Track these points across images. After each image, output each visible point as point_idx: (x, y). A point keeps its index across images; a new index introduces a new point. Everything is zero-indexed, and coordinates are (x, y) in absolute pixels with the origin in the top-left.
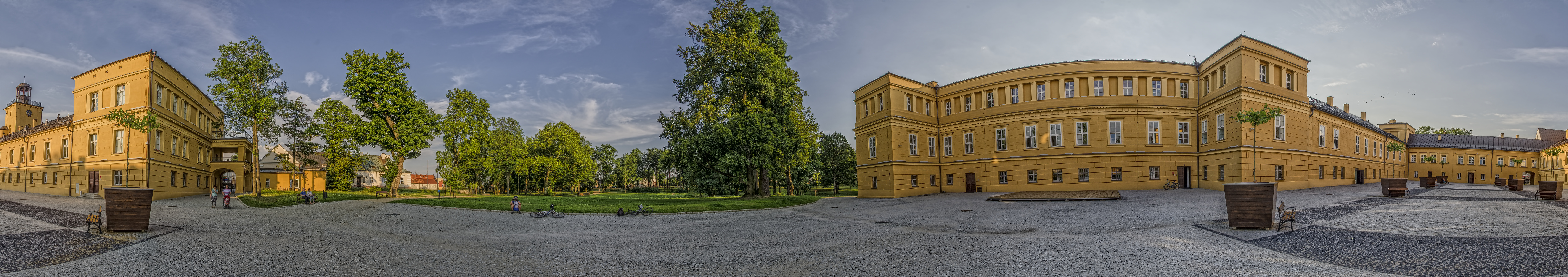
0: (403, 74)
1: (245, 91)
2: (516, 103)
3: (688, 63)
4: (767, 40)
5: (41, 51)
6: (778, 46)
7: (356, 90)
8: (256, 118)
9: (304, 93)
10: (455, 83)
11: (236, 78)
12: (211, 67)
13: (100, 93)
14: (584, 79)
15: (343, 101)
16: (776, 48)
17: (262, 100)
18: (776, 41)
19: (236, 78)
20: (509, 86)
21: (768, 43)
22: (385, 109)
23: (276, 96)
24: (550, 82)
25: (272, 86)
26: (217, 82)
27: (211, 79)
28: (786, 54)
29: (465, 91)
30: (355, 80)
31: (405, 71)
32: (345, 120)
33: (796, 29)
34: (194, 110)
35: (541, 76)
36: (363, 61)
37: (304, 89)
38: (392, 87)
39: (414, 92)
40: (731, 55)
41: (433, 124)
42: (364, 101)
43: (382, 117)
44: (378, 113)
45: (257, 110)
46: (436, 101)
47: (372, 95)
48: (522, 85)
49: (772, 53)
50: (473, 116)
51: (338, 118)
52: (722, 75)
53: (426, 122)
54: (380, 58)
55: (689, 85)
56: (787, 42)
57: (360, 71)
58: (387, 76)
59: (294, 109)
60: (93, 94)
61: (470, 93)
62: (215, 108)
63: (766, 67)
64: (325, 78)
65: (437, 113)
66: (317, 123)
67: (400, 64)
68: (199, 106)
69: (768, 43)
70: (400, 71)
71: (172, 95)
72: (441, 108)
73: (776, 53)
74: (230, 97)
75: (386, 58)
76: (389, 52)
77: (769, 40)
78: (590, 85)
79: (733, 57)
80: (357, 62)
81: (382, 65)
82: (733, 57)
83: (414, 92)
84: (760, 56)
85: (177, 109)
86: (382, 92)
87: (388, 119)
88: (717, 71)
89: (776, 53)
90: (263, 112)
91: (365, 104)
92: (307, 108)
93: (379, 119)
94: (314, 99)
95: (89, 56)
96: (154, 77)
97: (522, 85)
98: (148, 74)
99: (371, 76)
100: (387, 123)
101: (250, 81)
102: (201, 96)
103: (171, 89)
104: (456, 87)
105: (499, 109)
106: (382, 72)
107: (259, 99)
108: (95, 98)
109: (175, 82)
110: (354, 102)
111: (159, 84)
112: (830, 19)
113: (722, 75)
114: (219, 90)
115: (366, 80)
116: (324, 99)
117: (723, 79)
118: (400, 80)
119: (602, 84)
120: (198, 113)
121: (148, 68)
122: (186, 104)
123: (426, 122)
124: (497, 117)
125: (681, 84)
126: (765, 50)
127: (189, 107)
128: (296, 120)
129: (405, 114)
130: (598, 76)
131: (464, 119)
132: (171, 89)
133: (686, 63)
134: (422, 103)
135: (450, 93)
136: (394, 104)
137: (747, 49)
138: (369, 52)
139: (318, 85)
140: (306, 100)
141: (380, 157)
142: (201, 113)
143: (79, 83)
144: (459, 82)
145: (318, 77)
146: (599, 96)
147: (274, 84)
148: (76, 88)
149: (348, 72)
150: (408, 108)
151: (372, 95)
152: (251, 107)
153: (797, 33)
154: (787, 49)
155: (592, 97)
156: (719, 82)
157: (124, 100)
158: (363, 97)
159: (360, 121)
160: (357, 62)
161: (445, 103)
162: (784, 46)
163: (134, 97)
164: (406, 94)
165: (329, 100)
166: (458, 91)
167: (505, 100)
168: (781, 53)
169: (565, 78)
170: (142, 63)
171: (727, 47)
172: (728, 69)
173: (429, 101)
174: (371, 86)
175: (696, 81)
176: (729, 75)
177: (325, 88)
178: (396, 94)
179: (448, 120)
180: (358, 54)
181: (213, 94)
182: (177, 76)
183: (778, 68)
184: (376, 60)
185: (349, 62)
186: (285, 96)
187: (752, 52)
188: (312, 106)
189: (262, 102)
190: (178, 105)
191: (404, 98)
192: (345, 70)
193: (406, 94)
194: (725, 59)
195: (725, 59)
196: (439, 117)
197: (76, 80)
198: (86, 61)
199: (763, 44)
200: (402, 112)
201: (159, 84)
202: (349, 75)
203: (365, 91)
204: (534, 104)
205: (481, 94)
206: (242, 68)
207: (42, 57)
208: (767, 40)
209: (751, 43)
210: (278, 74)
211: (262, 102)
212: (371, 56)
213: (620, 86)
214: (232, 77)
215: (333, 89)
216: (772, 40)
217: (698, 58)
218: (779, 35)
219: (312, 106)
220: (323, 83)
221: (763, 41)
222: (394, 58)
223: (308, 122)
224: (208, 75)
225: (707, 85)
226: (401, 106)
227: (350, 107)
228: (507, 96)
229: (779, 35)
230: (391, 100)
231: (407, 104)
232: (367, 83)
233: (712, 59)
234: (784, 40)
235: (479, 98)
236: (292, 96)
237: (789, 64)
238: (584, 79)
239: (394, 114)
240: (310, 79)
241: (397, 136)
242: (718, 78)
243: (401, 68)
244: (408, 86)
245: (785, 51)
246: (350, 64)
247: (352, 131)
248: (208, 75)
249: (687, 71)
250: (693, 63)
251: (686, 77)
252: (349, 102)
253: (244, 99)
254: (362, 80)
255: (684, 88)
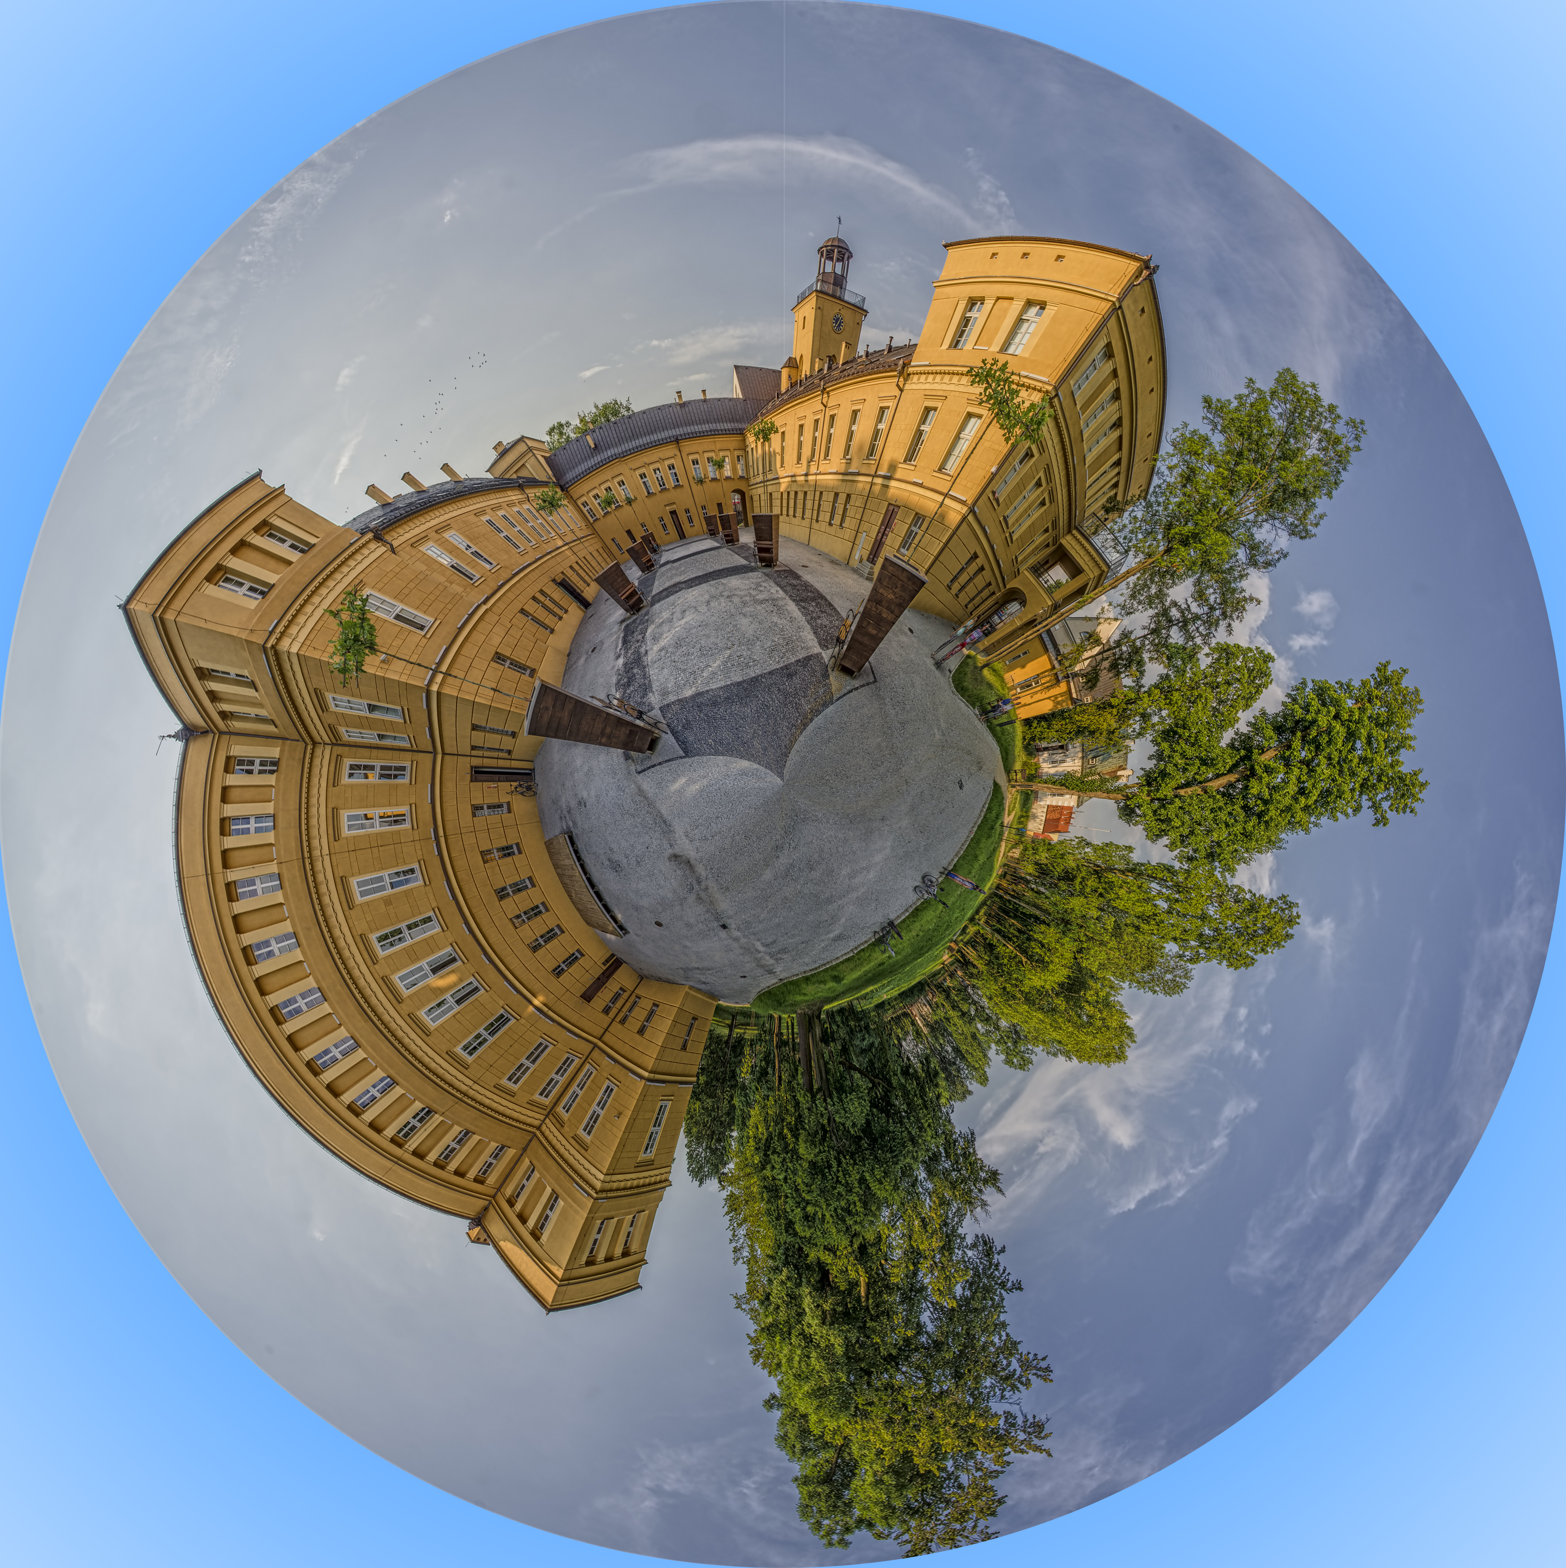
0: (1357, 809)
1: (1221, 494)
2: (1217, 1019)
3: (1010, 1347)
4: (830, 1454)
5: (887, 154)
6: (800, 1437)
7: (1306, 708)
8: (1168, 551)
9: (1272, 604)
10: (1317, 921)
11: (1240, 454)
12: (1229, 389)
13: (989, 304)
14: (1188, 1175)
15: (1273, 687)
16: (805, 1432)
17: (1219, 537)
18: (804, 1450)
19: (1240, 454)
20: (1266, 1029)
21: (826, 1445)
22: (1259, 770)
23: (1242, 555)
24: (1231, 1110)
25: (1263, 534)
26: (1205, 429)
27: (1201, 412)
28: (777, 1414)
29: (1288, 936)
30: (1336, 703)
31: (1367, 814)
32: (1221, 702)
33: (749, 1486)
34: (1115, 447)
35: (1253, 1104)
36: (1391, 713)
37: (1284, 601)
38: (1321, 785)
39: (1307, 831)
40: (916, 1399)
41: (1211, 856)
42: (1279, 729)
43: (1235, 766)
44: (1248, 757)
45: (1197, 541)
46: (1274, 874)
47: (1297, 743)
48: (1255, 1055)
49: (813, 1418)
50: (1216, 930)
51: (1222, 689)
52: (923, 1339)
53: (1219, 844)
54: (1404, 755)
55: (987, 1290)
56: (774, 1450)
57: (1362, 710)
58: (1353, 774)
59: (1224, 602)
60: (972, 302)
61: (1278, 944)
62: (1146, 473)
63: (826, 1377)
64: (1327, 635)
65: (1241, 868)
66: (1200, 656)
67: (1385, 805)
68: (1130, 445)
69: (826, 1445)
70: (1365, 803)
71: (1111, 387)
72: (1253, 878)
73: (804, 1416)
74: (1188, 478)
75: (1404, 769)
76: (1421, 778)
77: (824, 1455)
78: (1165, 1172)
79: (909, 1393)
80: (1386, 700)
81: (1382, 760)
82: (909, 1393)
83: (1307, 831)
84: (844, 1406)
85: (1093, 425)
86: (1307, 763)
87: (1232, 778)
88: (938, 1345)
89: (804, 1416)
90: (1192, 553)
91: (1270, 732)
92: (1236, 624)
93: (1230, 762)
94: (1263, 629)
95: (1003, 198)
96: (1112, 323)
97: (1255, 1055)
98: (1105, 307)
99: (1351, 736)
100: (1218, 776)
101: (1251, 484)
102: (1153, 429)
103: (1122, 373)
104: (1305, 920)
105: (1215, 984)
106: (1363, 760)
107: (1218, 529)
108: (973, 314)
109: (1140, 361)
110: (1273, 709)
111: (1109, 345)
112: (650, 1503)
113: (923, 1339)
114: (1192, 446)
115: (1339, 729)
116: (1269, 650)
117: (920, 1328)
118: (1340, 803)
119: (1147, 1192)
120: (1115, 458)
121: (1114, 296)
122: (1118, 424)
123: (1219, 844)
124: (1197, 969)
125: (1003, 1285)
126: (832, 1425)
127: (1115, 434)
128: (1197, 617)
129: (1245, 808)
130: (1170, 1202)
131: (1211, 911)
132: (1122, 373)
133: (1015, 1344)
134: (1272, 844)
135: (1291, 905)
136: (1275, 788)
137: (879, 1423)
138: (1416, 727)
139: (1306, 625)
140: (1254, 616)
141: (1122, 768)
142: (1118, 463)
143: (961, 262)
144: (1316, 932)
145: (1327, 620)
146: (1129, 1163)
147: (1270, 538)
148: (944, 274)
149: (1356, 684)
150: (1260, 816)
151: (1297, 743)
152: (1190, 526)
153: (749, 1474)
154: (775, 1430)
155: (1138, 1150)
156: (925, 1317)
157: (1021, 347)
158: (1290, 727)
159: (1222, 728)
160: (1386, 700)
161: (1266, 888)
162: (784, 1438)
163: (1039, 351)
164: (1300, 815)
165: (1268, 658)
166: (1291, 921)
167: (1236, 1002)
168: (791, 1417)
169: (1217, 1143)
170: (1109, 274)
171: (931, 1417)
172: (915, 1357)
173: (1276, 857)
174: (1324, 739)
175: (975, 1304)
176: (907, 1341)
177: (1299, 642)
178: (1302, 792)
179: (1218, 884)
180: (1411, 700)
181: (1174, 445)
182: (1154, 352)
183: (797, 1376)
184: (1396, 747)
185: (1384, 679)
186: (1251, 570)
187: (866, 1415)
188: (1243, 632)
189: (1213, 537)
190: (1101, 416)
191: (1289, 809)
192: (1360, 674)
193: (1300, 815)
194: (929, 1383)
195: (929, 1383)
196: (1232, 871)
197: (952, 252)
198: (990, 209)
199: (839, 1442)
200: (1251, 803)
201: (1109, 345)
202: (1346, 687)
203: (1306, 729)
204: (1197, 1049)
205: (1268, 966)
206: (1272, 448)
207: (890, 172)
208: (830, 1454)
209: (871, 1442)
210: (1299, 531)
211: (1213, 537)
212: (1408, 731)
213: (1114, 1211)
214: (1238, 445)
215: (1299, 660)
216: (815, 1454)
217: (993, 1369)
218: (796, 1469)
219: (1243, 632)
220: (1311, 634)
221: (840, 1450)
222: (1405, 789)
223: (1198, 640)
224: (1207, 401)
225: (951, 1304)
226: (1266, 802)
227: (1257, 706)
228: (1243, 1012)
229: (796, 1469)
230: (1286, 782)
231: (1273, 813)
232: (1329, 731)
233: (958, 1376)
234: (783, 1455)
235: (1260, 957)
236: (1257, 584)
237: (772, 1386)
238: (1188, 1175)
239: (1246, 788)
240: (1315, 603)
241: (1182, 792)
242: (930, 1328)
243: (1375, 807)
244: (1324, 820)
245: (782, 1423)
246: (1379, 685)
247: (1193, 718)
248: (1207, 401)
249: (1004, 1325)
250: (1000, 1351)
251: (998, 1307)
252: (1272, 699)
253: (1202, 504)
254: (1337, 717)
255: (991, 1277)
